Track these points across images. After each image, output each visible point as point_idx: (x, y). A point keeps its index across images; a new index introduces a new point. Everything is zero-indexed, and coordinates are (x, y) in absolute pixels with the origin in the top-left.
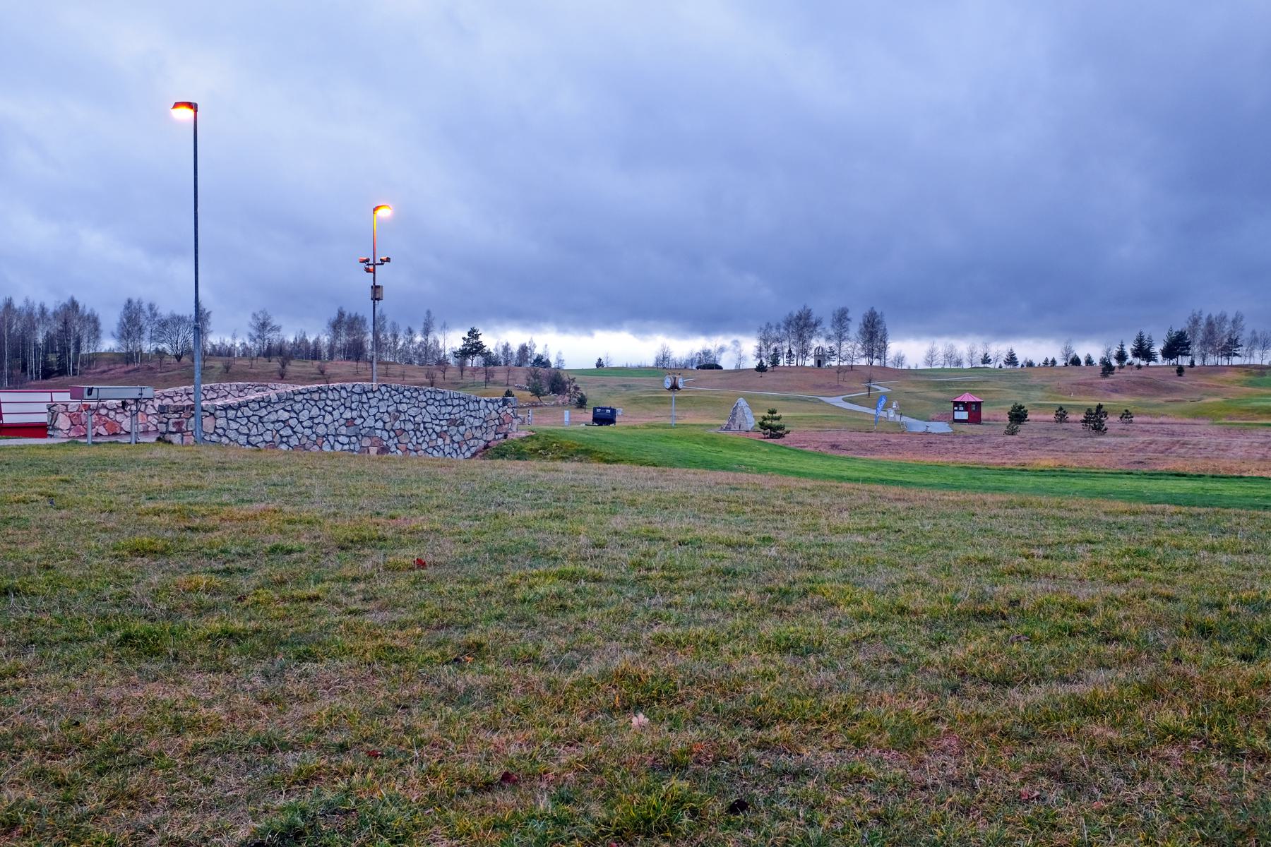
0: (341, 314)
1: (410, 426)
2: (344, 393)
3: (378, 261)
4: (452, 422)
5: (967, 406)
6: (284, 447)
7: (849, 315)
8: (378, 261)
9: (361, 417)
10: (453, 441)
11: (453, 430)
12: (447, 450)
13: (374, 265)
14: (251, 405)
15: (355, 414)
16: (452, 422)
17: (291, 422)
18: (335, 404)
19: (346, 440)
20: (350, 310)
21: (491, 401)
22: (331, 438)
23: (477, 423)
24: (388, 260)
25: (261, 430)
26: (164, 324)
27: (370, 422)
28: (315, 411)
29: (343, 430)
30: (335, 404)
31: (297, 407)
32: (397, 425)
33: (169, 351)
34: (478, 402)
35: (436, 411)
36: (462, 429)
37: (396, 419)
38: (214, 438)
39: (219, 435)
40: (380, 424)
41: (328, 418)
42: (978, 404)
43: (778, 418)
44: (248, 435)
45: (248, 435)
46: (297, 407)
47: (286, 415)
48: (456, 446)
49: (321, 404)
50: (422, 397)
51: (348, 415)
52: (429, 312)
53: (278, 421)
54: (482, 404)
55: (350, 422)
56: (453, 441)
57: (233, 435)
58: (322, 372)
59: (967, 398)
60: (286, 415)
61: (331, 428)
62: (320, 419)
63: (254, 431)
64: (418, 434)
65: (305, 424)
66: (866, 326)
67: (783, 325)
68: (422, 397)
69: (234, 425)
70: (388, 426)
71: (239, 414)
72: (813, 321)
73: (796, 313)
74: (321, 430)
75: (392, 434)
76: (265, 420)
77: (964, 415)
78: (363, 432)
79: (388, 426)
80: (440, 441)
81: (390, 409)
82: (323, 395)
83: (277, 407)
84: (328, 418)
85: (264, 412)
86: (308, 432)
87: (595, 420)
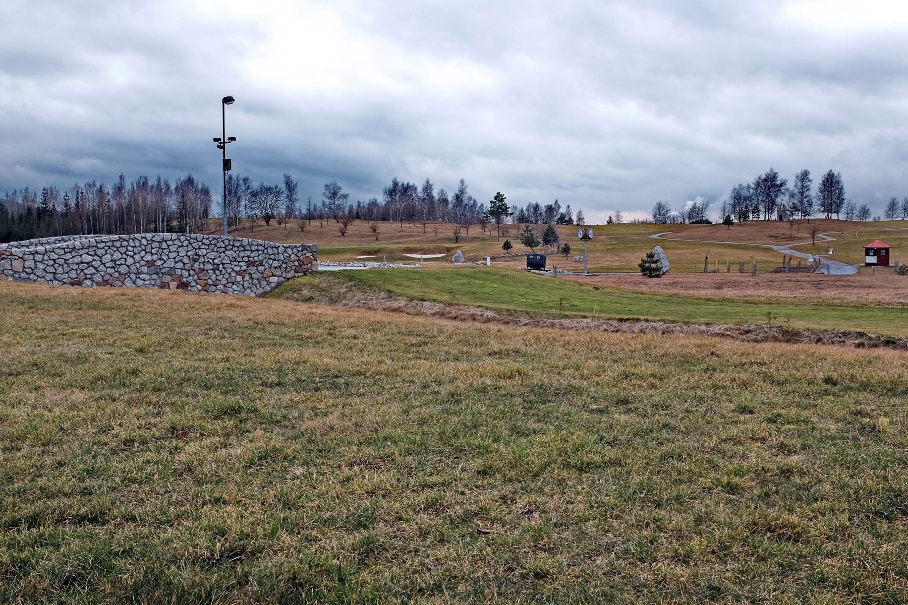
0: (395, 184)
1: (210, 267)
2: (144, 242)
3: (227, 140)
4: (250, 263)
5: (877, 252)
6: (88, 283)
7: (810, 177)
8: (227, 140)
9: (161, 259)
10: (252, 278)
11: (252, 269)
12: (246, 285)
13: (224, 143)
14: (57, 251)
15: (155, 257)
16: (250, 263)
17: (94, 263)
18: (136, 250)
19: (147, 277)
20: (200, 180)
21: (290, 247)
22: (133, 276)
23: (276, 264)
24: (234, 139)
25: (66, 269)
26: (255, 195)
27: (171, 263)
28: (117, 255)
29: (145, 269)
30: (136, 250)
31: (99, 252)
32: (196, 265)
33: (259, 214)
34: (277, 248)
35: (235, 255)
36: (261, 268)
37: (195, 261)
38: (23, 275)
39: (27, 273)
40: (180, 265)
41: (130, 261)
42: (887, 250)
43: (656, 262)
44: (55, 273)
45: (55, 273)
46: (99, 252)
47: (90, 258)
48: (255, 281)
49: (123, 250)
50: (221, 244)
51: (148, 257)
52: (462, 182)
53: (82, 263)
54: (281, 249)
55: (150, 264)
56: (252, 278)
57: (40, 273)
58: (375, 231)
59: (876, 244)
60: (90, 258)
61: (133, 268)
62: (123, 261)
63: (60, 270)
64: (218, 272)
65: (107, 265)
66: (824, 185)
67: (753, 186)
68: (221, 244)
69: (40, 266)
70: (188, 266)
71: (46, 257)
72: (778, 183)
73: (764, 176)
74: (123, 269)
75: (192, 272)
76: (70, 261)
77: (873, 259)
78: (163, 271)
79: (188, 266)
80: (239, 278)
81: (189, 254)
82: (125, 243)
83: (81, 252)
84: (130, 261)
85: (69, 256)
86: (110, 271)
87: (528, 265)
